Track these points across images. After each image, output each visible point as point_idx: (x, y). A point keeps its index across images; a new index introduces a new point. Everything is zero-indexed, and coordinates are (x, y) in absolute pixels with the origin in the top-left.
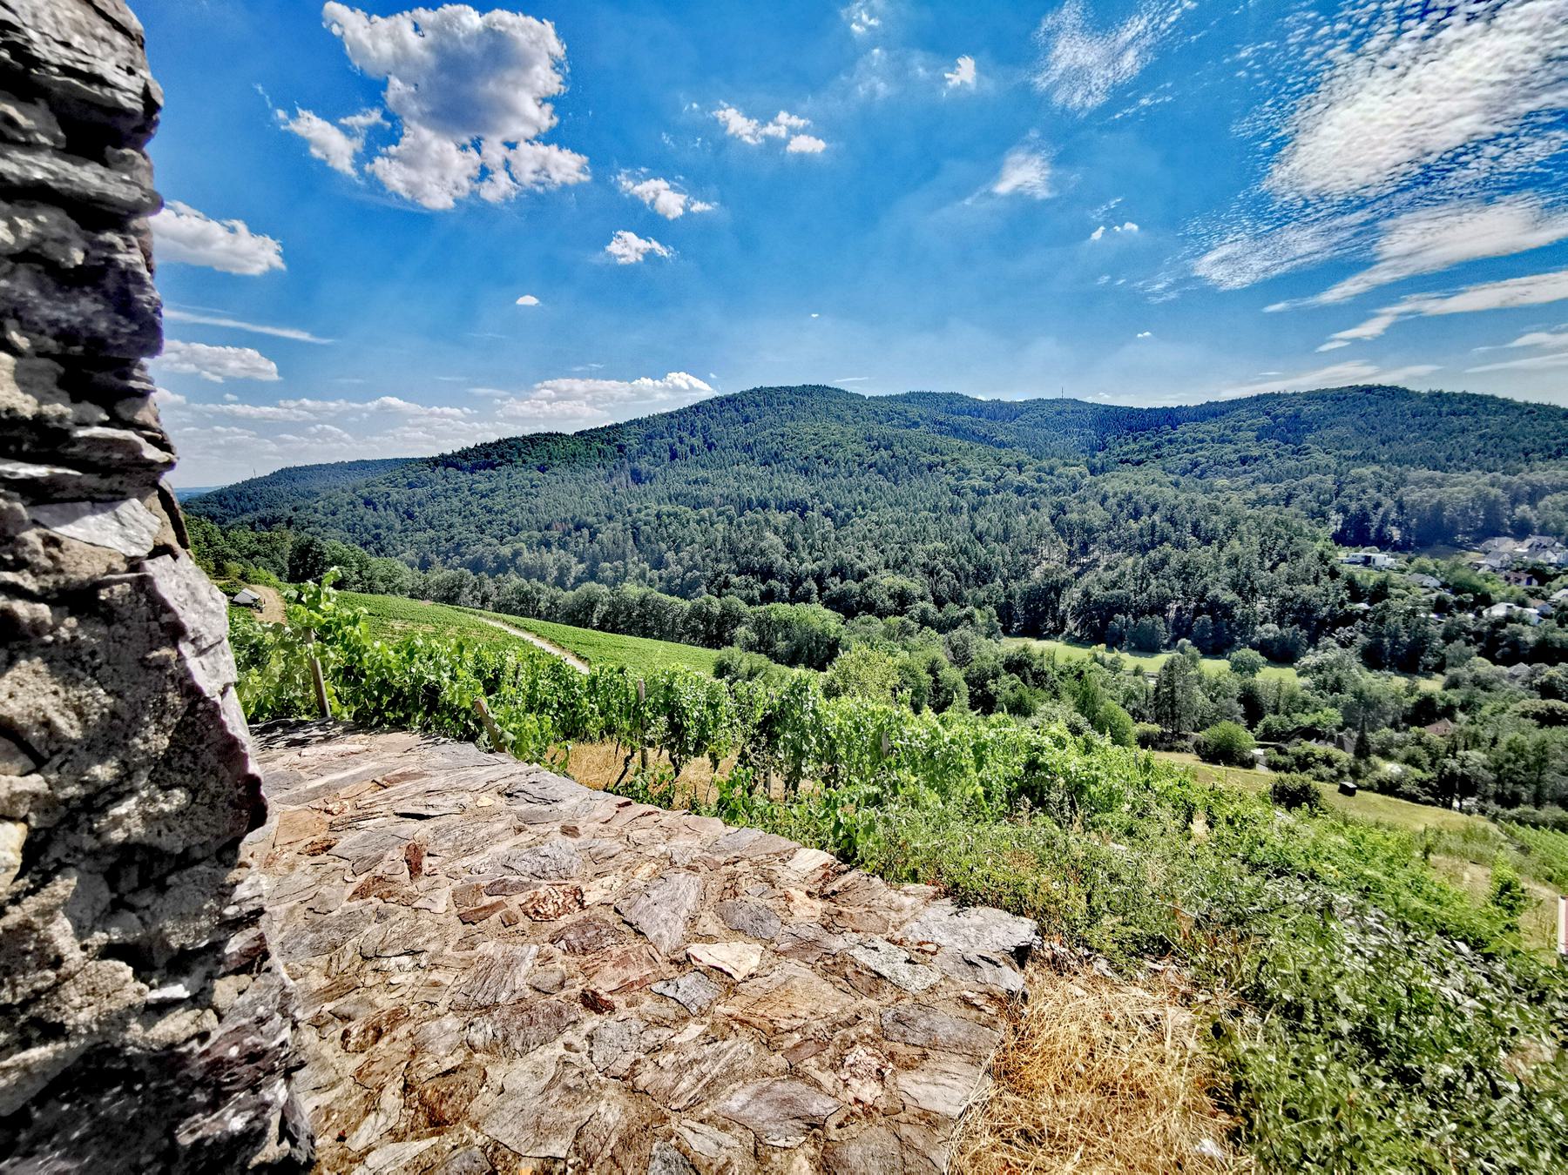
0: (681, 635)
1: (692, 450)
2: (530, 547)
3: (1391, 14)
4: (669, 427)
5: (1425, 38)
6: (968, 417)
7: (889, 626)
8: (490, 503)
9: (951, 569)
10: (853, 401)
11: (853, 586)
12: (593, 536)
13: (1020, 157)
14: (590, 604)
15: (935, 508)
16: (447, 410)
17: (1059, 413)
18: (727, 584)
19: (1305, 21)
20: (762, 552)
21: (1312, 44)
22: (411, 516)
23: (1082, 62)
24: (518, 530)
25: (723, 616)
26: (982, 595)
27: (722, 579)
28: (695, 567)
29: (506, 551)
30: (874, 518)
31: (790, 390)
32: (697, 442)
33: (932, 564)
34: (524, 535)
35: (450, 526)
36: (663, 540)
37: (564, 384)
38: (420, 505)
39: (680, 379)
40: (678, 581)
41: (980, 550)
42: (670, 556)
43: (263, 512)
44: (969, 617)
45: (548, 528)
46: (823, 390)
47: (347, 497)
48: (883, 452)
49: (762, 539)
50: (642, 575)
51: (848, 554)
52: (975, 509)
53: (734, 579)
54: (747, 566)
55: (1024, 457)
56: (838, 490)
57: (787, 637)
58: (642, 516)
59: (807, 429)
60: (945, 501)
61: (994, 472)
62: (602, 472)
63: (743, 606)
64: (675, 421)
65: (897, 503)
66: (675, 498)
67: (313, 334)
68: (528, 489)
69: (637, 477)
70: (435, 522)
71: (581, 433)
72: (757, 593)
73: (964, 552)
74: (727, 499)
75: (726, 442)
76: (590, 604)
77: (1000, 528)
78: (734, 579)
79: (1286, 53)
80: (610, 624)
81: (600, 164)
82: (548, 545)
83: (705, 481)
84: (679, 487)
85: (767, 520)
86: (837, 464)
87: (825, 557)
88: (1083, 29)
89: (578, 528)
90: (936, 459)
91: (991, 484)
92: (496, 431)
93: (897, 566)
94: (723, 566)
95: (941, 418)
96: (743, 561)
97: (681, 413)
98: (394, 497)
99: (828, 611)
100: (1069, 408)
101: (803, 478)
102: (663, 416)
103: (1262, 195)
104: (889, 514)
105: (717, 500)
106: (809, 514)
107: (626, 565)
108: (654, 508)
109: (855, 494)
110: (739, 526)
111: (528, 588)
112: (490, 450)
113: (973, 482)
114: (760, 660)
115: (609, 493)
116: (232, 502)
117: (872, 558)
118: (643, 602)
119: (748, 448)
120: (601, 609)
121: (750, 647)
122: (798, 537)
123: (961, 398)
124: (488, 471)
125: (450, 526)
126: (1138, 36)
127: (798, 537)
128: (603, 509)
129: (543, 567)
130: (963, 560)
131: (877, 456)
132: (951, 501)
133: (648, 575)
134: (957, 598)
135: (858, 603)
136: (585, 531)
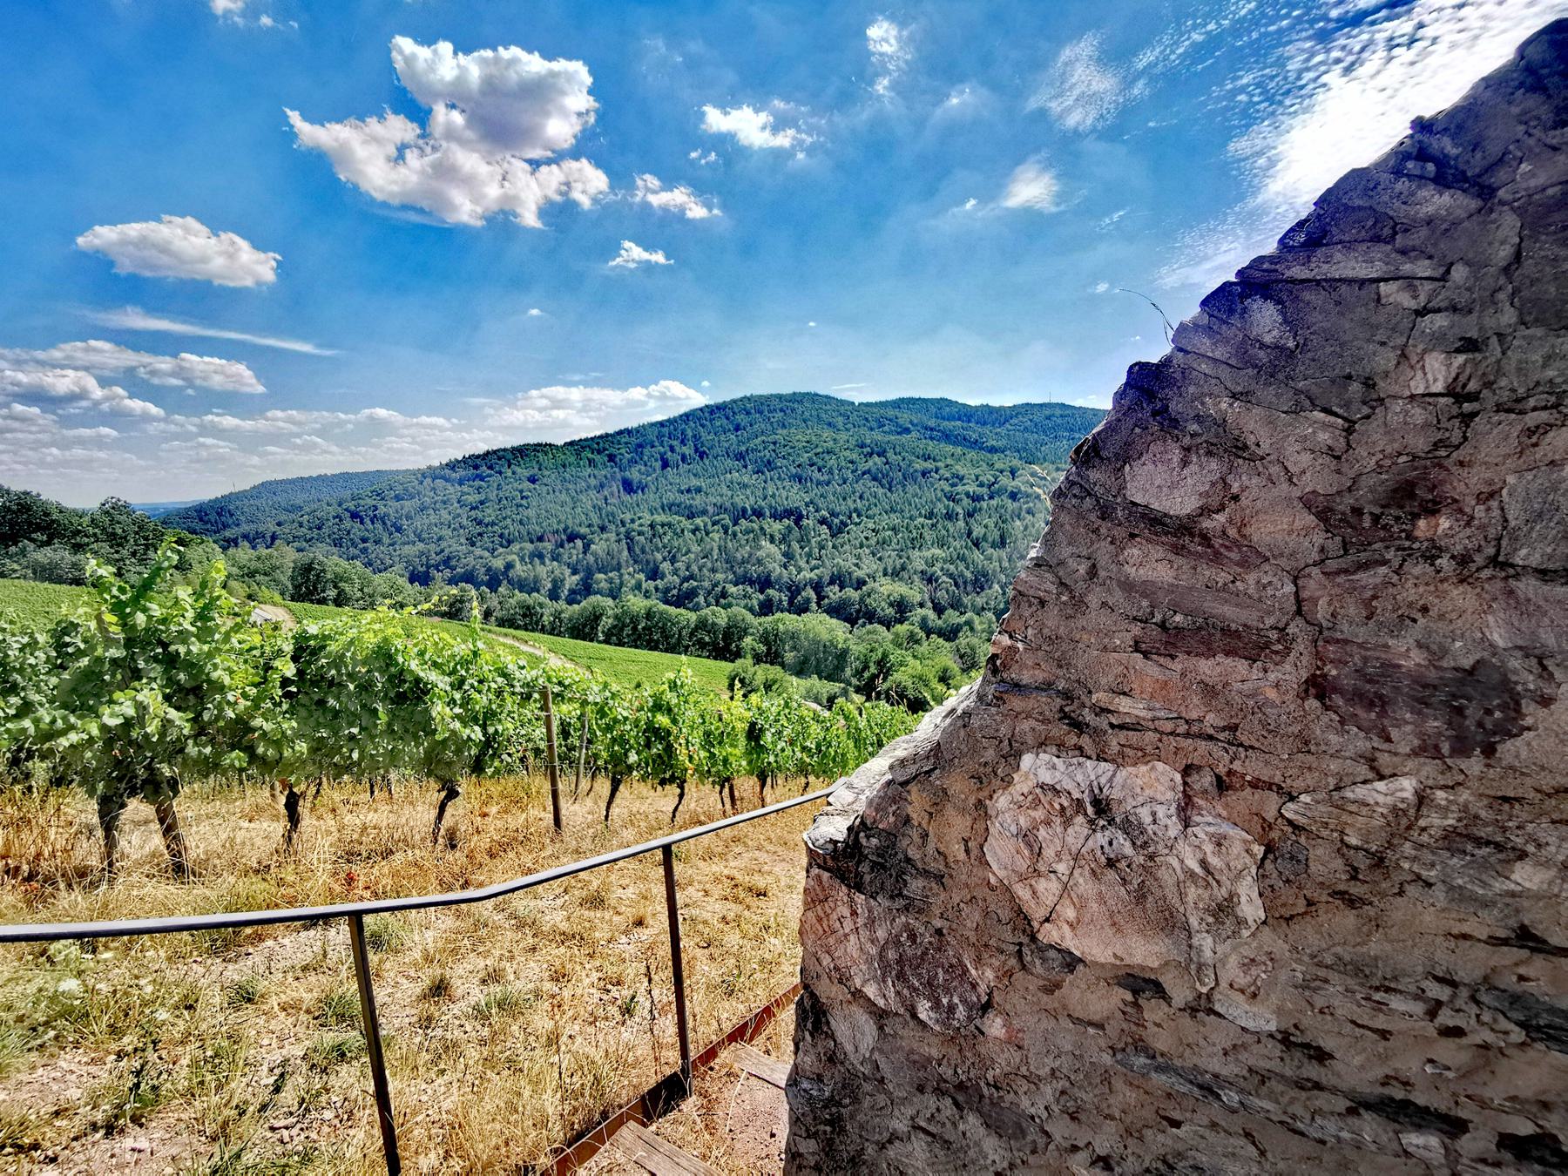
0: (687, 647)
1: (684, 458)
2: (522, 559)
3: (1382, 45)
4: (660, 436)
5: (1413, 63)
6: (959, 423)
7: (897, 635)
8: (480, 515)
9: (951, 576)
10: (845, 409)
11: (852, 594)
12: (586, 547)
13: (1031, 175)
14: (596, 617)
15: (930, 515)
16: (424, 419)
17: (1048, 418)
18: (724, 595)
19: (1304, 50)
20: (760, 562)
21: (1308, 69)
22: (399, 530)
23: (1081, 85)
24: (509, 542)
25: (729, 627)
26: (980, 601)
27: (719, 589)
28: (692, 577)
29: (498, 564)
30: (871, 525)
31: (780, 397)
32: (688, 450)
33: (930, 571)
34: (515, 547)
35: (440, 539)
36: (658, 550)
37: (559, 391)
38: (408, 518)
39: (676, 388)
40: (675, 592)
41: (977, 556)
42: (666, 567)
43: (245, 528)
44: (969, 623)
45: (540, 539)
46: (813, 397)
47: (332, 510)
48: (876, 459)
49: (760, 548)
50: (638, 586)
51: (845, 562)
52: (970, 515)
53: (732, 589)
54: (745, 577)
55: (1016, 463)
56: (833, 500)
57: (794, 648)
58: (635, 526)
59: (799, 437)
60: (940, 508)
61: (988, 477)
62: (593, 482)
63: (749, 617)
64: (665, 430)
65: (893, 510)
66: (670, 507)
67: (319, 346)
68: (518, 500)
69: (628, 486)
70: (425, 535)
71: (572, 443)
72: (755, 602)
73: (962, 558)
74: (721, 508)
75: (717, 450)
76: (596, 617)
77: (996, 535)
78: (732, 589)
79: (1286, 78)
80: (615, 637)
81: (620, 177)
82: (541, 556)
83: (699, 490)
84: (672, 496)
85: (762, 529)
86: (831, 472)
87: (823, 565)
88: (1099, 60)
89: (571, 538)
90: (929, 465)
91: (985, 490)
92: (484, 440)
93: (896, 574)
94: (720, 576)
95: (931, 423)
96: (740, 571)
97: (671, 421)
98: (382, 510)
99: (834, 621)
100: (1058, 412)
101: (797, 486)
102: (652, 425)
103: (1258, 208)
104: (885, 521)
105: (711, 509)
106: (805, 522)
107: (621, 576)
108: (647, 518)
109: (850, 502)
110: (735, 535)
111: (531, 602)
112: (478, 462)
113: (967, 488)
114: (775, 672)
115: (601, 503)
116: (213, 517)
117: (869, 565)
118: (649, 615)
119: (740, 457)
120: (607, 622)
121: (758, 659)
122: (795, 546)
123: (950, 403)
124: (477, 483)
125: (440, 539)
126: (1150, 66)
127: (795, 546)
128: (596, 520)
129: (536, 580)
130: (962, 567)
131: (870, 463)
132: (947, 507)
133: (644, 585)
134: (957, 605)
135: (858, 611)
136: (579, 543)
